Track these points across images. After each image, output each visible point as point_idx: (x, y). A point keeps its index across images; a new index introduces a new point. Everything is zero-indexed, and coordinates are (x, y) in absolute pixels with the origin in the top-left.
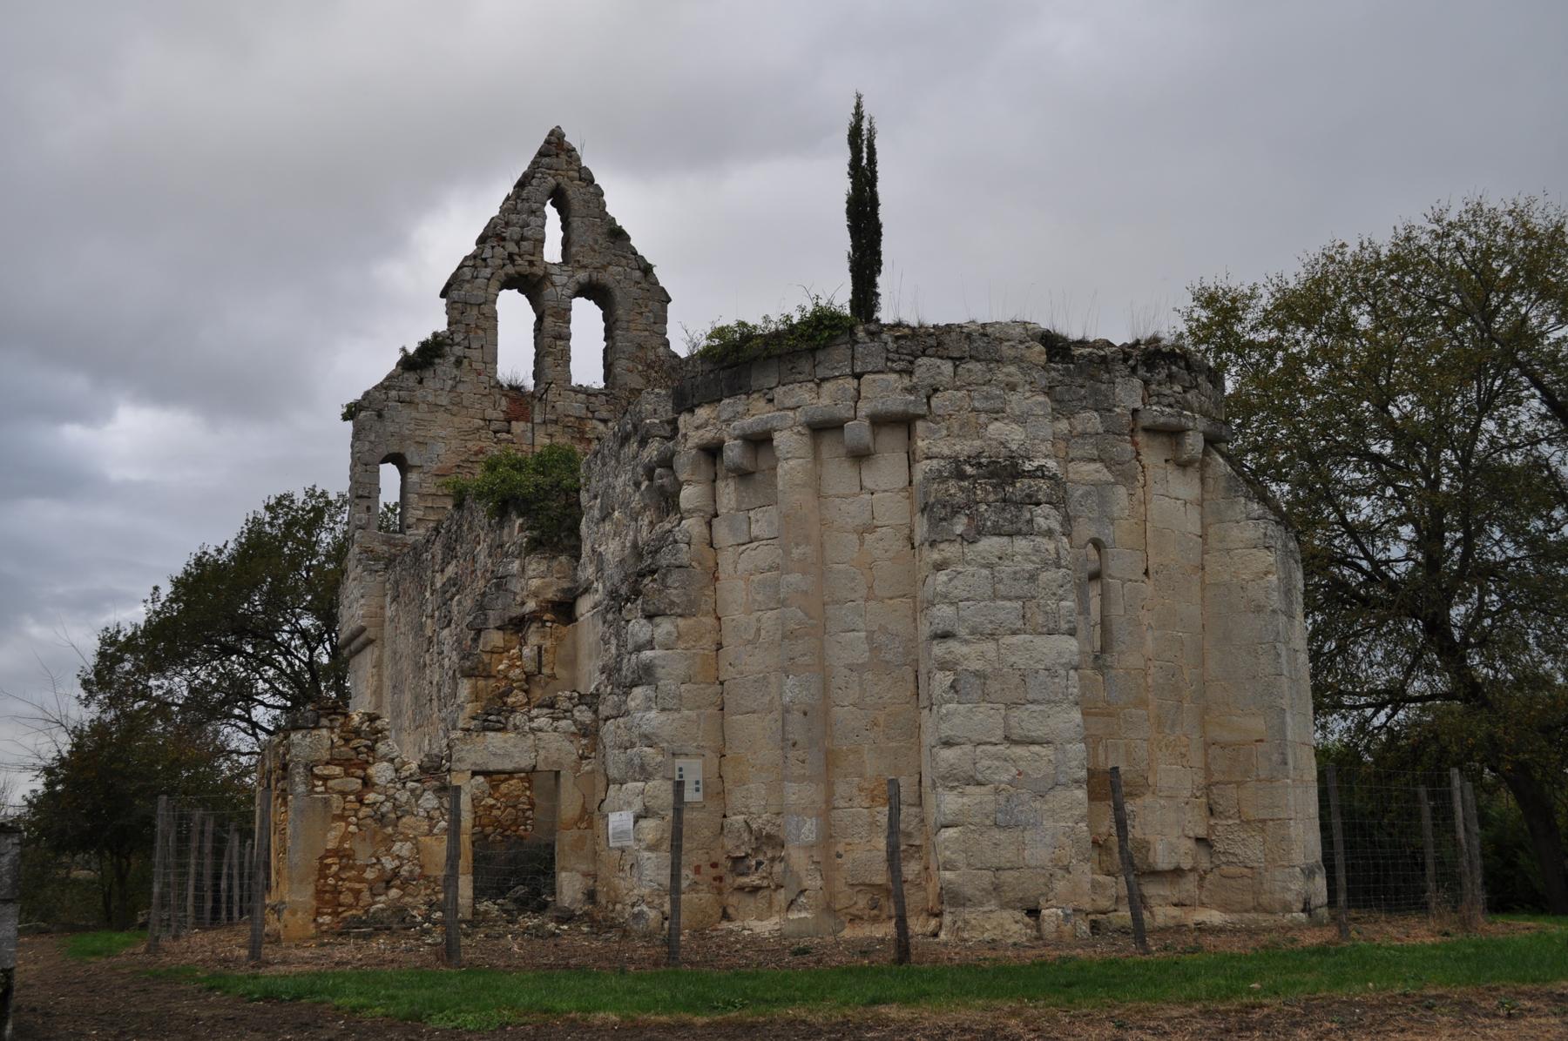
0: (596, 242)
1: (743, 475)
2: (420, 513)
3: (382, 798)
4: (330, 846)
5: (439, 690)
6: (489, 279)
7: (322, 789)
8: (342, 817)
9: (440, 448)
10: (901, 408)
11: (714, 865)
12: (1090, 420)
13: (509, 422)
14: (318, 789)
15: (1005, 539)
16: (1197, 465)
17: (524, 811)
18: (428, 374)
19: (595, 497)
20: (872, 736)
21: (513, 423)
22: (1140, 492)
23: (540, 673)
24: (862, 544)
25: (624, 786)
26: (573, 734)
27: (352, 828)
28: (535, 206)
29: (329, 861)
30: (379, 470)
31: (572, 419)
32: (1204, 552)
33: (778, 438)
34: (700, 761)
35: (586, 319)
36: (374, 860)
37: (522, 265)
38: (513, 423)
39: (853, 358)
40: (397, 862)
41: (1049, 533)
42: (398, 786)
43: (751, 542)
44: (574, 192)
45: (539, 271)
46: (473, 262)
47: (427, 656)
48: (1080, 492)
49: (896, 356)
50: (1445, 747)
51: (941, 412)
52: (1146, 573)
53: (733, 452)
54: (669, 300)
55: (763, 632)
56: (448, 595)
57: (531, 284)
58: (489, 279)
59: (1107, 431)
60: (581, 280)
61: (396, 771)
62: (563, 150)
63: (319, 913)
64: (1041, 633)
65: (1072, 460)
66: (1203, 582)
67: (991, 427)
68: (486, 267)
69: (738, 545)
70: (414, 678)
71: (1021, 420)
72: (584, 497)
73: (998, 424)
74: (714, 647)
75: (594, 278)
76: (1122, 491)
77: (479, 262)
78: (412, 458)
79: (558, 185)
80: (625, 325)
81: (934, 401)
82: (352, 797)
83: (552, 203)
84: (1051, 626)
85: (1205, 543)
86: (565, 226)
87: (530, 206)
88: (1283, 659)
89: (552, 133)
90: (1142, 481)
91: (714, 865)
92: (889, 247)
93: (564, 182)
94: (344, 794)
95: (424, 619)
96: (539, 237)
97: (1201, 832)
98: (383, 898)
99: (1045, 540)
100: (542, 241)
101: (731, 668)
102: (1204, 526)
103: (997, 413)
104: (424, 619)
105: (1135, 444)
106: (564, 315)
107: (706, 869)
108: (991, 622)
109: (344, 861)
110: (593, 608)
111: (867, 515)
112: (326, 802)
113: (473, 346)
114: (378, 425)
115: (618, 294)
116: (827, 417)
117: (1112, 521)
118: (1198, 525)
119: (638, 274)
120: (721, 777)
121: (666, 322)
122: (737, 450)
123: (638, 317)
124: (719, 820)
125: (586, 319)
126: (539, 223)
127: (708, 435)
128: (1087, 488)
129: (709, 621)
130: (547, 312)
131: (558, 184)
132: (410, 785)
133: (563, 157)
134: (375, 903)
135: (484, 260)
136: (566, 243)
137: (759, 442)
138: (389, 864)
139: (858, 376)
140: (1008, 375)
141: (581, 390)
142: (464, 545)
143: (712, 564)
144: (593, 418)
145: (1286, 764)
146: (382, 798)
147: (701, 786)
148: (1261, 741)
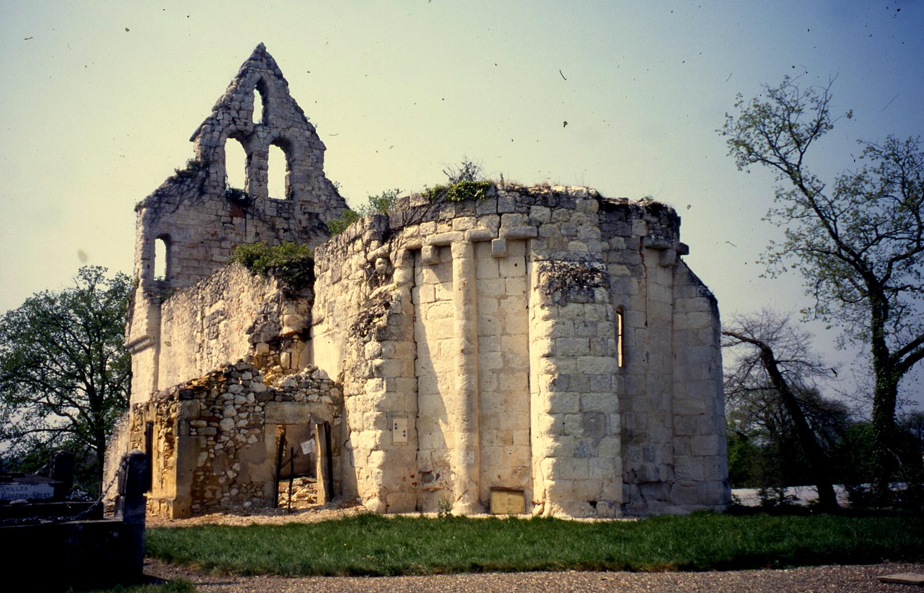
1: (432, 265)
2: (179, 270)
3: (228, 439)
7: (195, 433)
8: (207, 449)
9: (192, 232)
10: (523, 232)
11: (413, 476)
13: (232, 218)
14: (193, 434)
15: (580, 305)
20: (504, 408)
22: (643, 281)
23: (290, 368)
24: (499, 304)
25: (361, 433)
26: (330, 404)
27: (212, 456)
28: (248, 90)
30: (154, 243)
33: (453, 246)
34: (406, 420)
35: (276, 157)
37: (240, 125)
39: (497, 204)
40: (235, 475)
41: (603, 302)
43: (436, 301)
44: (270, 83)
45: (250, 129)
46: (211, 122)
50: (43, 453)
51: (543, 235)
52: (646, 324)
53: (427, 252)
55: (442, 351)
56: (217, 320)
57: (245, 137)
58: (221, 132)
59: (628, 248)
60: (275, 135)
62: (265, 57)
63: (193, 503)
64: (598, 356)
65: (610, 263)
68: (219, 125)
69: (428, 303)
70: (187, 367)
71: (586, 241)
73: (572, 242)
74: (413, 358)
75: (282, 135)
76: (634, 281)
77: (214, 121)
78: (175, 237)
80: (300, 163)
82: (212, 438)
84: (604, 352)
86: (265, 102)
89: (259, 47)
91: (413, 476)
93: (265, 77)
94: (207, 436)
96: (251, 108)
97: (670, 461)
98: (228, 494)
99: (601, 306)
100: (252, 111)
103: (573, 237)
104: (195, 333)
105: (642, 255)
106: (264, 156)
107: (408, 478)
108: (573, 349)
110: (326, 332)
111: (503, 289)
112: (197, 441)
115: (296, 145)
116: (482, 236)
117: (630, 295)
118: (671, 299)
120: (416, 429)
123: (307, 158)
124: (415, 452)
125: (276, 157)
126: (250, 100)
127: (413, 243)
128: (617, 278)
129: (411, 345)
130: (254, 153)
131: (262, 78)
132: (242, 431)
134: (223, 497)
135: (218, 120)
136: (265, 113)
137: (442, 248)
138: (231, 474)
139: (500, 215)
140: (579, 216)
141: (275, 201)
143: (412, 312)
146: (228, 439)
147: (406, 433)
148: (703, 414)
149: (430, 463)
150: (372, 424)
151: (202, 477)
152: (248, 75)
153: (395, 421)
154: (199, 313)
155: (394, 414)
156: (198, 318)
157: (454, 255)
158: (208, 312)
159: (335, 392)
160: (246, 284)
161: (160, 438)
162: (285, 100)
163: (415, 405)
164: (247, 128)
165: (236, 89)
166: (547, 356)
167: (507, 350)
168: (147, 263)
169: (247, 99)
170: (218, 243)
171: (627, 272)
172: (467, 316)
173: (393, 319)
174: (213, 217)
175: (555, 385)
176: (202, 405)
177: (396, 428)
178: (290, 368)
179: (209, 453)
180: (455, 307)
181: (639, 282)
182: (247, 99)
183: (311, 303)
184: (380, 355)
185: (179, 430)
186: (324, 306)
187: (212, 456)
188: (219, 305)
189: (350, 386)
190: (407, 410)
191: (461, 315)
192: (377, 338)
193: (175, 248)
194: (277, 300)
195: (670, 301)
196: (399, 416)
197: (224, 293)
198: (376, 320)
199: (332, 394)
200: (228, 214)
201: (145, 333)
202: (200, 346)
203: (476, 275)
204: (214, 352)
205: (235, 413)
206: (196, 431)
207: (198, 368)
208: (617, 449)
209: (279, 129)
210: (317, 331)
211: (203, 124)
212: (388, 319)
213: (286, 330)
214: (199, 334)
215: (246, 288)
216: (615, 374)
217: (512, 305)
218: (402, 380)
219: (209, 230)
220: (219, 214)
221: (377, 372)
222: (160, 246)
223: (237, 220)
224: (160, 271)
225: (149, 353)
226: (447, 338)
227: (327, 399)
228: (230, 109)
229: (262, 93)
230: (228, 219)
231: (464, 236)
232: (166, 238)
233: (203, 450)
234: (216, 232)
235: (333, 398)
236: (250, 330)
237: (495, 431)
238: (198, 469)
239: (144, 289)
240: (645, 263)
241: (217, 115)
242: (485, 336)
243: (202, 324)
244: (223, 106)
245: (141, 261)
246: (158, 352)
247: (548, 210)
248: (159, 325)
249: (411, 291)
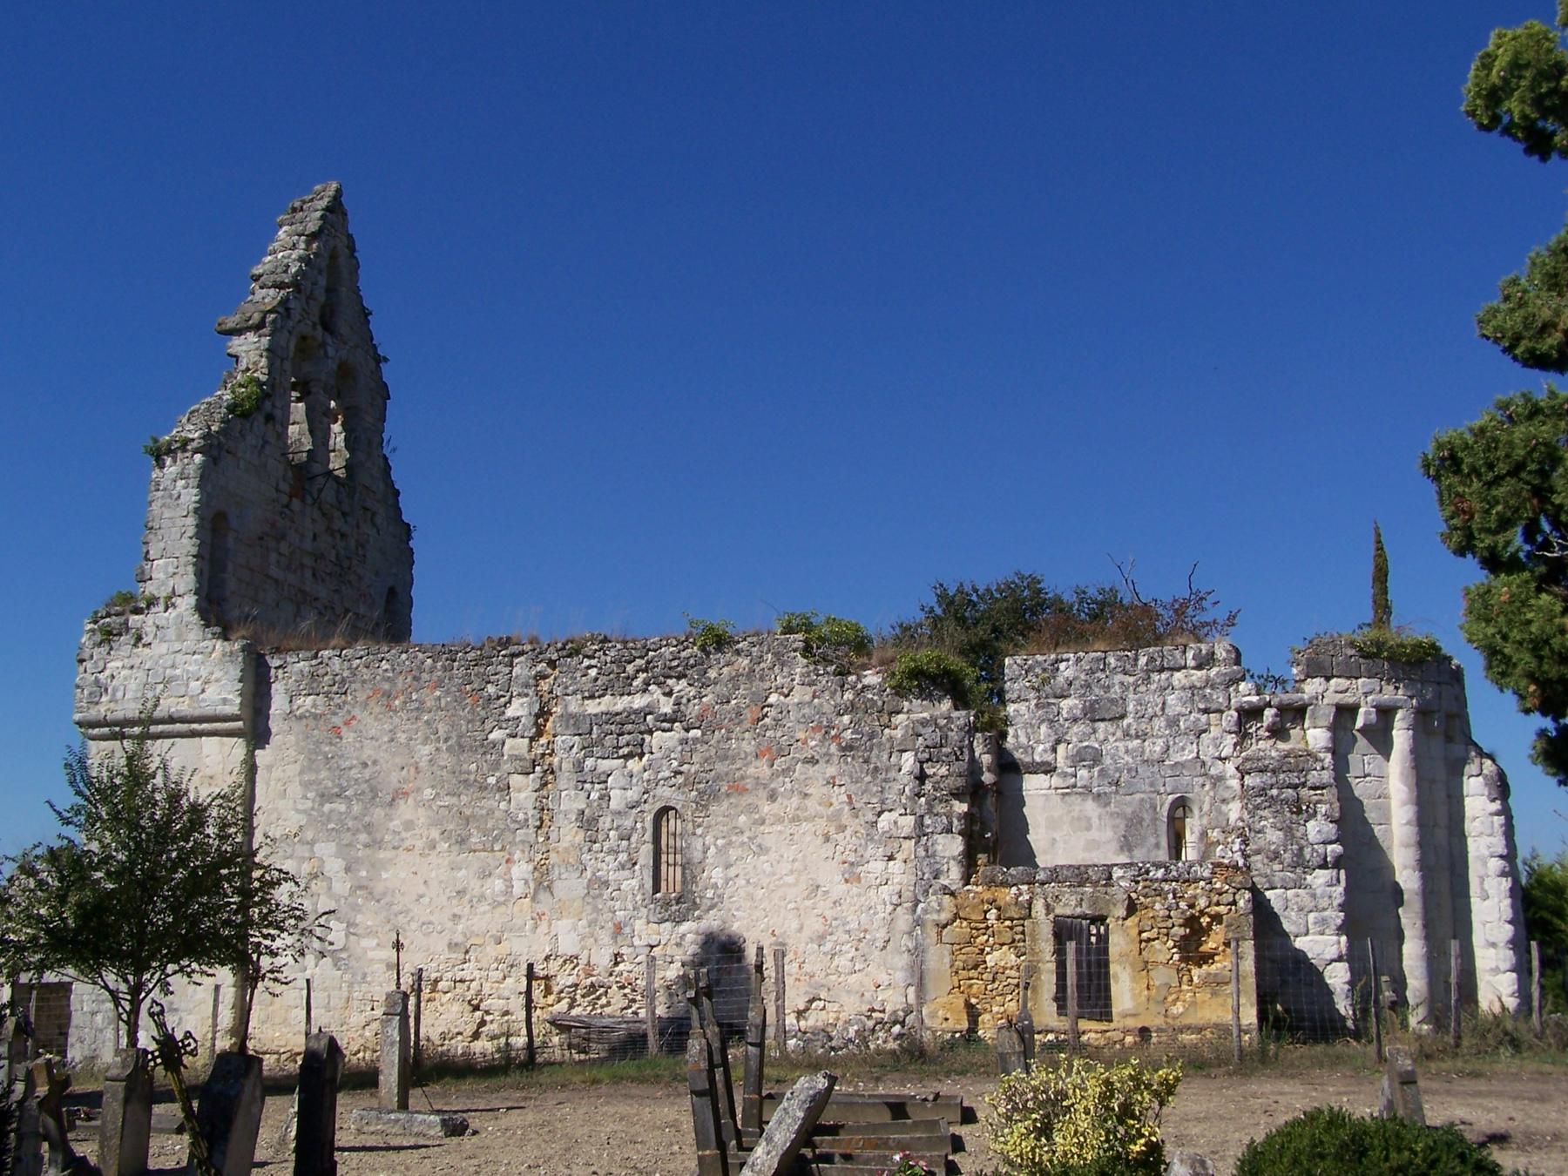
43: (1365, 777)
127: (1348, 699)
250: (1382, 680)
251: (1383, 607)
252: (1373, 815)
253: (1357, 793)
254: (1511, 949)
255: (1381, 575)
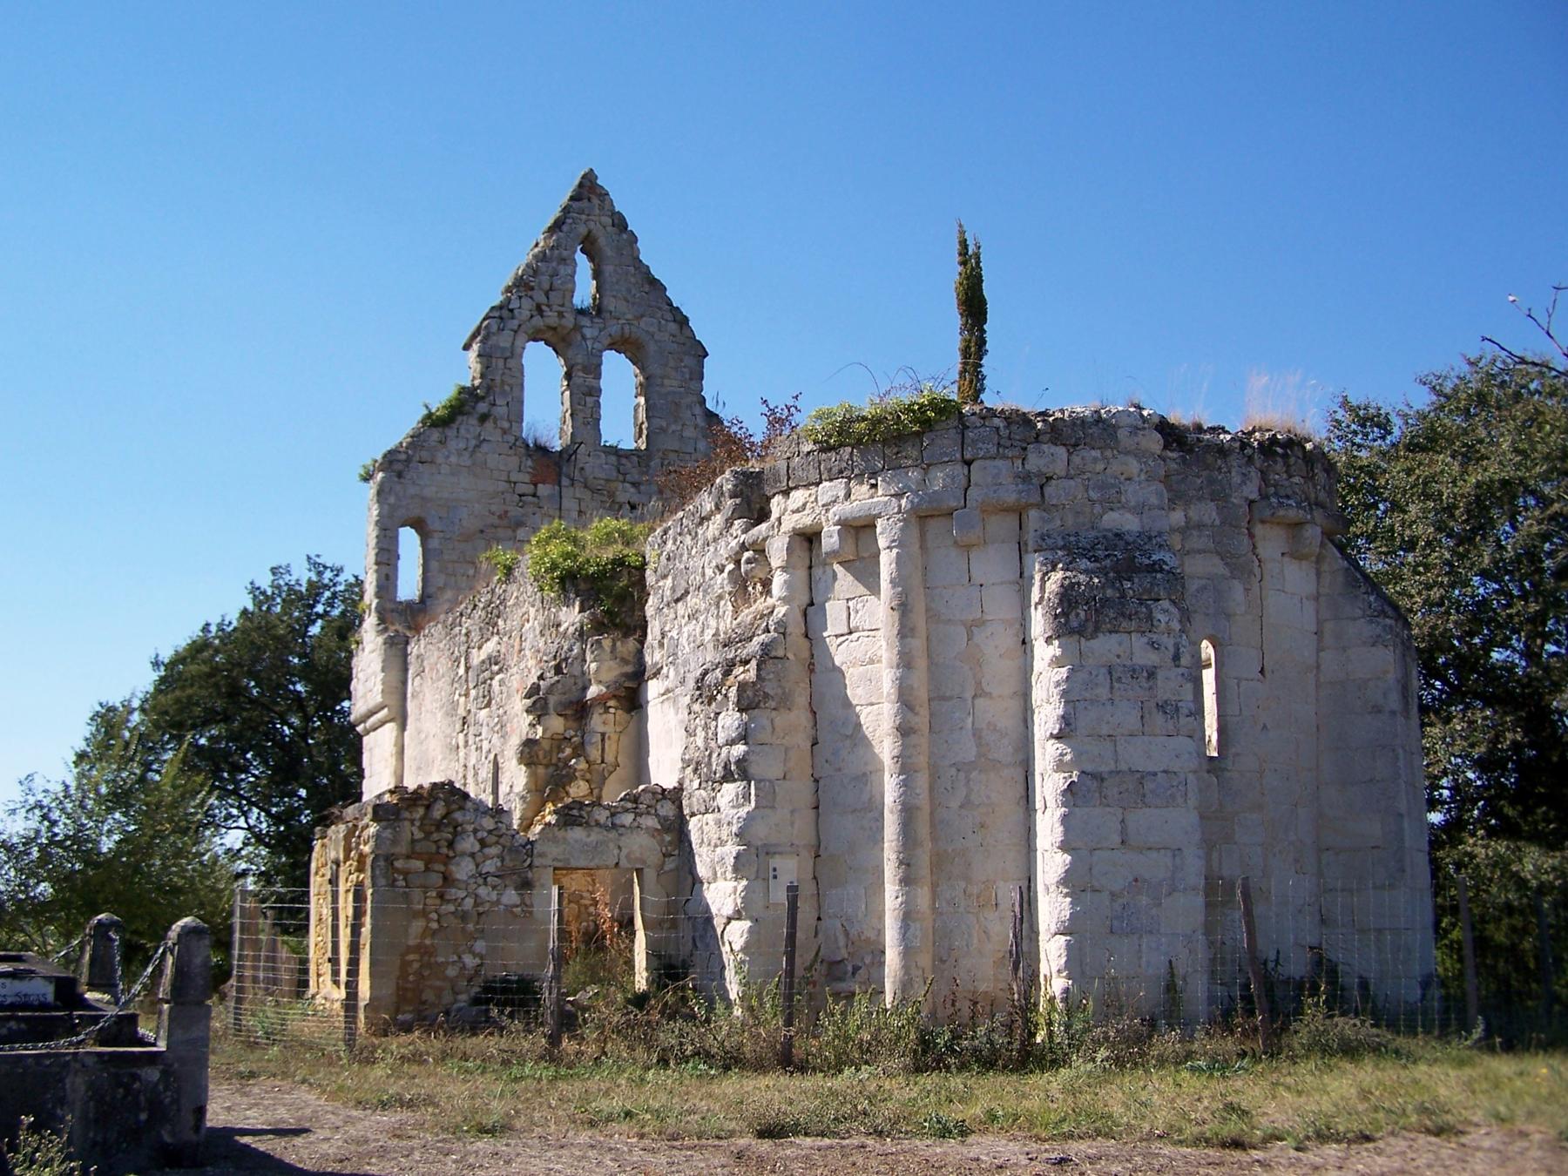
0: (629, 291)
3: (462, 894)
4: (412, 942)
5: (476, 774)
6: (516, 332)
8: (424, 914)
12: (1207, 512)
13: (535, 485)
16: (1313, 559)
17: (586, 907)
18: (451, 433)
19: (665, 577)
21: (540, 486)
28: (565, 253)
29: (411, 957)
31: (602, 482)
32: (1319, 650)
33: (880, 523)
36: (455, 958)
37: (551, 318)
38: (540, 486)
40: (477, 961)
42: (480, 881)
43: (851, 633)
46: (501, 314)
47: (461, 736)
48: (1195, 587)
49: (1008, 443)
52: (1262, 672)
53: (830, 539)
54: (706, 354)
57: (559, 342)
61: (477, 866)
65: (1188, 553)
66: (1317, 680)
67: (1105, 517)
68: (513, 318)
70: (444, 759)
72: (650, 577)
76: (1237, 587)
77: (505, 313)
78: (434, 524)
79: (590, 232)
81: (1048, 490)
83: (581, 250)
85: (1320, 640)
86: (597, 275)
87: (560, 254)
88: (1401, 763)
90: (1259, 577)
92: (993, 327)
94: (425, 888)
95: (457, 697)
96: (570, 286)
101: (827, 765)
102: (1319, 623)
104: (457, 697)
106: (595, 370)
109: (426, 958)
113: (498, 402)
114: (398, 488)
115: (652, 347)
117: (1228, 616)
119: (673, 327)
121: (702, 378)
122: (836, 538)
124: (814, 922)
127: (805, 520)
133: (596, 201)
135: (511, 311)
137: (859, 530)
139: (968, 463)
141: (614, 451)
142: (508, 622)
144: (624, 481)
145: (1404, 871)
148: (1377, 847)
149: (842, 941)
150: (730, 868)
151: (416, 965)
152: (565, 228)
153: (776, 862)
154: (463, 659)
155: (772, 850)
156: (461, 671)
157: (882, 542)
158: (477, 657)
159: (667, 809)
160: (533, 606)
161: (348, 891)
162: (632, 269)
163: (813, 833)
164: (564, 322)
165: (544, 253)
166: (1058, 737)
167: (984, 726)
168: (385, 569)
169: (563, 270)
170: (509, 533)
171: (1227, 572)
172: (905, 662)
173: (770, 666)
174: (503, 486)
175: (1073, 794)
176: (415, 829)
177: (775, 877)
178: (603, 762)
179: (429, 920)
180: (884, 643)
181: (1247, 590)
182: (563, 270)
183: (642, 640)
184: (744, 737)
185: (373, 877)
186: (661, 645)
187: (435, 925)
188: (490, 647)
189: (695, 794)
190: (796, 842)
191: (895, 659)
192: (738, 703)
193: (434, 543)
194: (581, 635)
195: (1313, 628)
196: (780, 853)
197: (500, 622)
198: (739, 670)
199: (662, 812)
200: (527, 478)
201: (379, 699)
202: (464, 721)
203: (925, 581)
204: (484, 730)
205: (477, 847)
206: (405, 879)
207: (462, 761)
208: (1199, 917)
209: (621, 322)
210: (654, 688)
211: (484, 319)
212: (759, 669)
213: (593, 691)
214: (463, 699)
215: (532, 611)
216: (1195, 772)
217: (996, 643)
218: (787, 784)
219: (494, 508)
220: (513, 479)
221: (739, 771)
222: (409, 541)
223: (543, 490)
224: (409, 586)
225: (390, 729)
226: (872, 704)
227: (650, 822)
228: (532, 289)
229: (591, 258)
230: (529, 489)
231: (900, 506)
232: (419, 525)
233: (416, 915)
234: (506, 512)
235: (663, 820)
236: (534, 691)
237: (963, 884)
238: (409, 950)
239: (379, 619)
240: (1260, 550)
241: (509, 300)
242: (944, 699)
243: (467, 681)
244: (521, 285)
245: (375, 567)
246: (403, 727)
247: (1061, 452)
248: (405, 683)
249: (805, 615)
250: (850, 479)
251: (974, 349)
252: (859, 691)
253: (837, 663)
254: (1066, 895)
255: (973, 306)
